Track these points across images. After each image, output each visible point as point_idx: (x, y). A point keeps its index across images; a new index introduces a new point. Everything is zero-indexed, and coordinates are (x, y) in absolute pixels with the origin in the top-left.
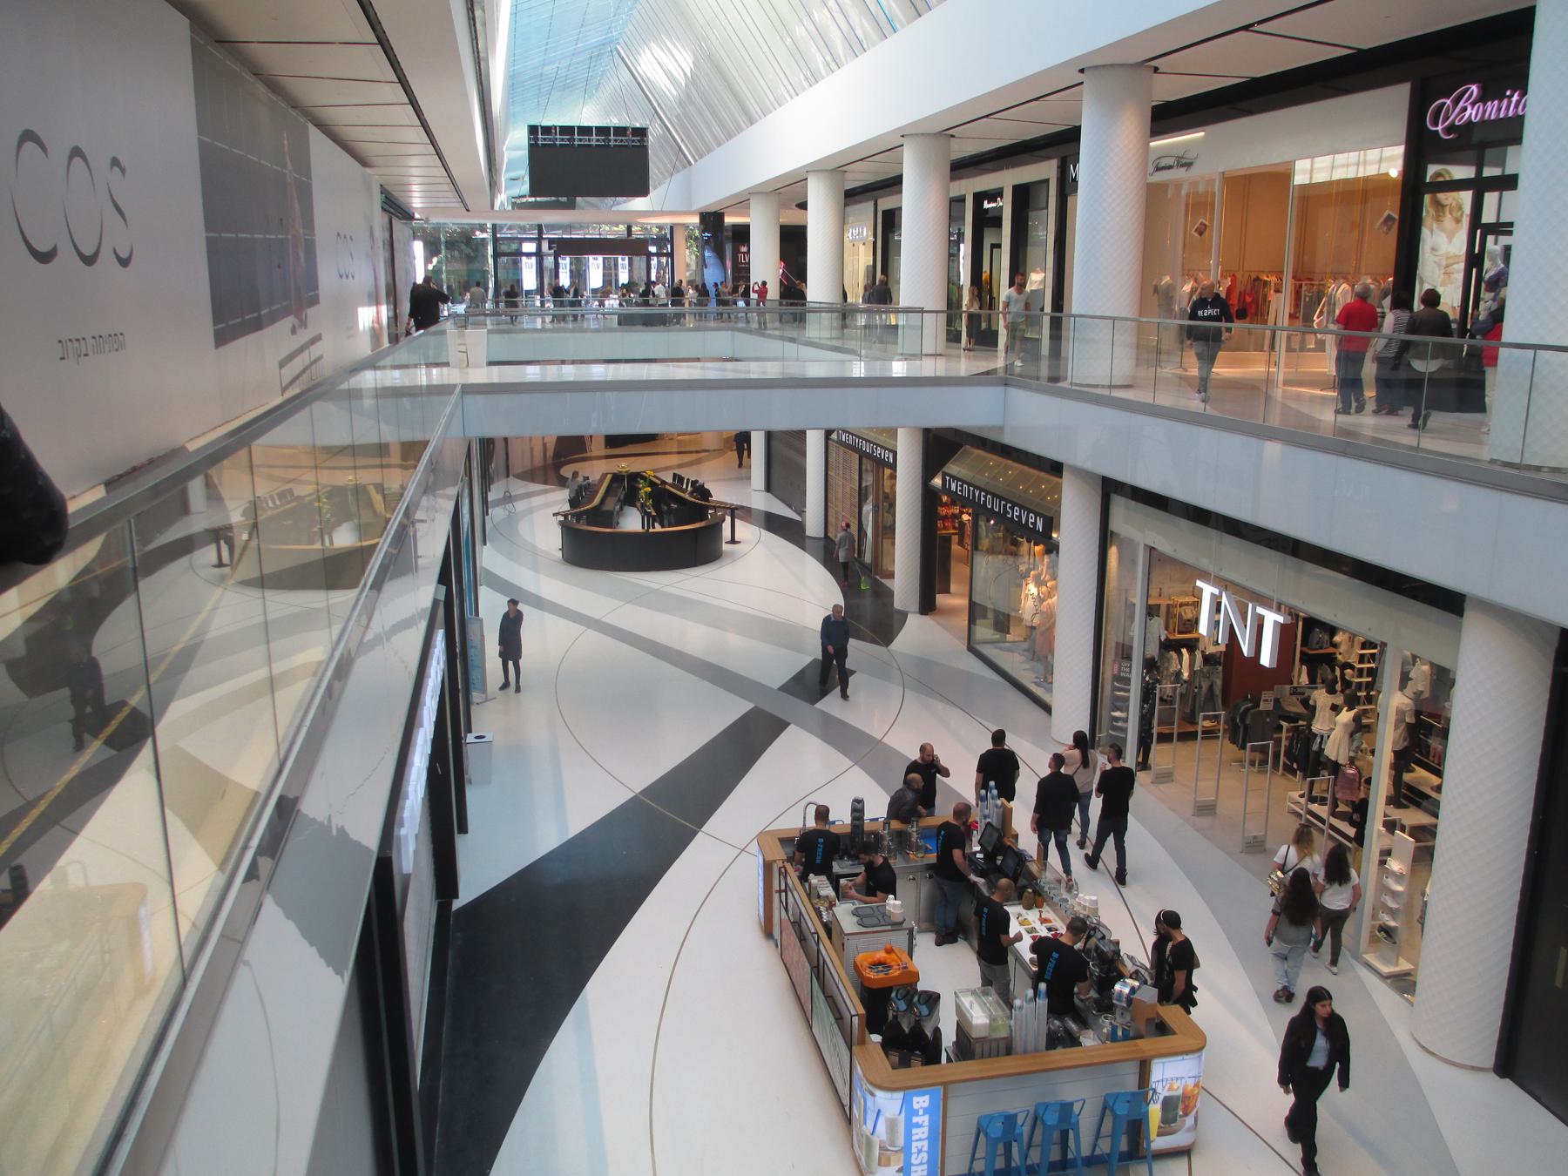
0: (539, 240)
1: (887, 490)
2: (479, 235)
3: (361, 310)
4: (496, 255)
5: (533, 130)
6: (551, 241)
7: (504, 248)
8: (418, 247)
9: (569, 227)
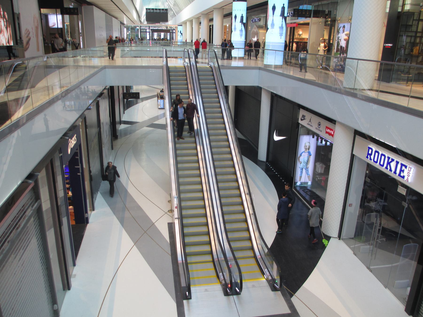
0: (149, 29)
1: (343, 44)
2: (138, 28)
3: (71, 194)
4: (141, 32)
5: (147, 9)
6: (151, 29)
7: (142, 31)
8: (125, 29)
9: (155, 27)
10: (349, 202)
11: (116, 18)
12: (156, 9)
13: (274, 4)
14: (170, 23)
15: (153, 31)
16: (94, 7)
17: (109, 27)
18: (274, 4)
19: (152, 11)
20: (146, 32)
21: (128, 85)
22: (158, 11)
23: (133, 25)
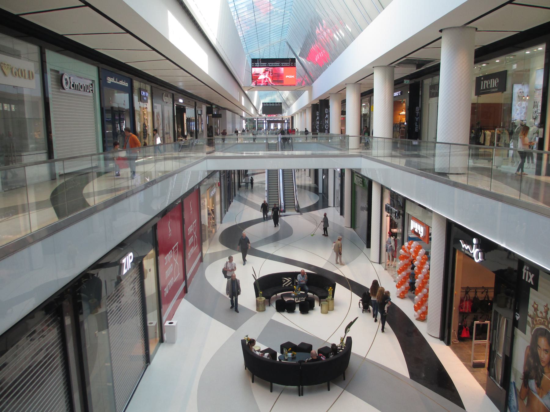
8: (244, 121)
10: (366, 213)
11: (237, 114)
12: (272, 103)
13: (525, 334)
14: (286, 115)
15: (270, 122)
16: (227, 111)
17: (234, 123)
18: (525, 334)
19: (267, 105)
20: (263, 123)
21: (246, 169)
22: (273, 105)
23: (250, 117)
